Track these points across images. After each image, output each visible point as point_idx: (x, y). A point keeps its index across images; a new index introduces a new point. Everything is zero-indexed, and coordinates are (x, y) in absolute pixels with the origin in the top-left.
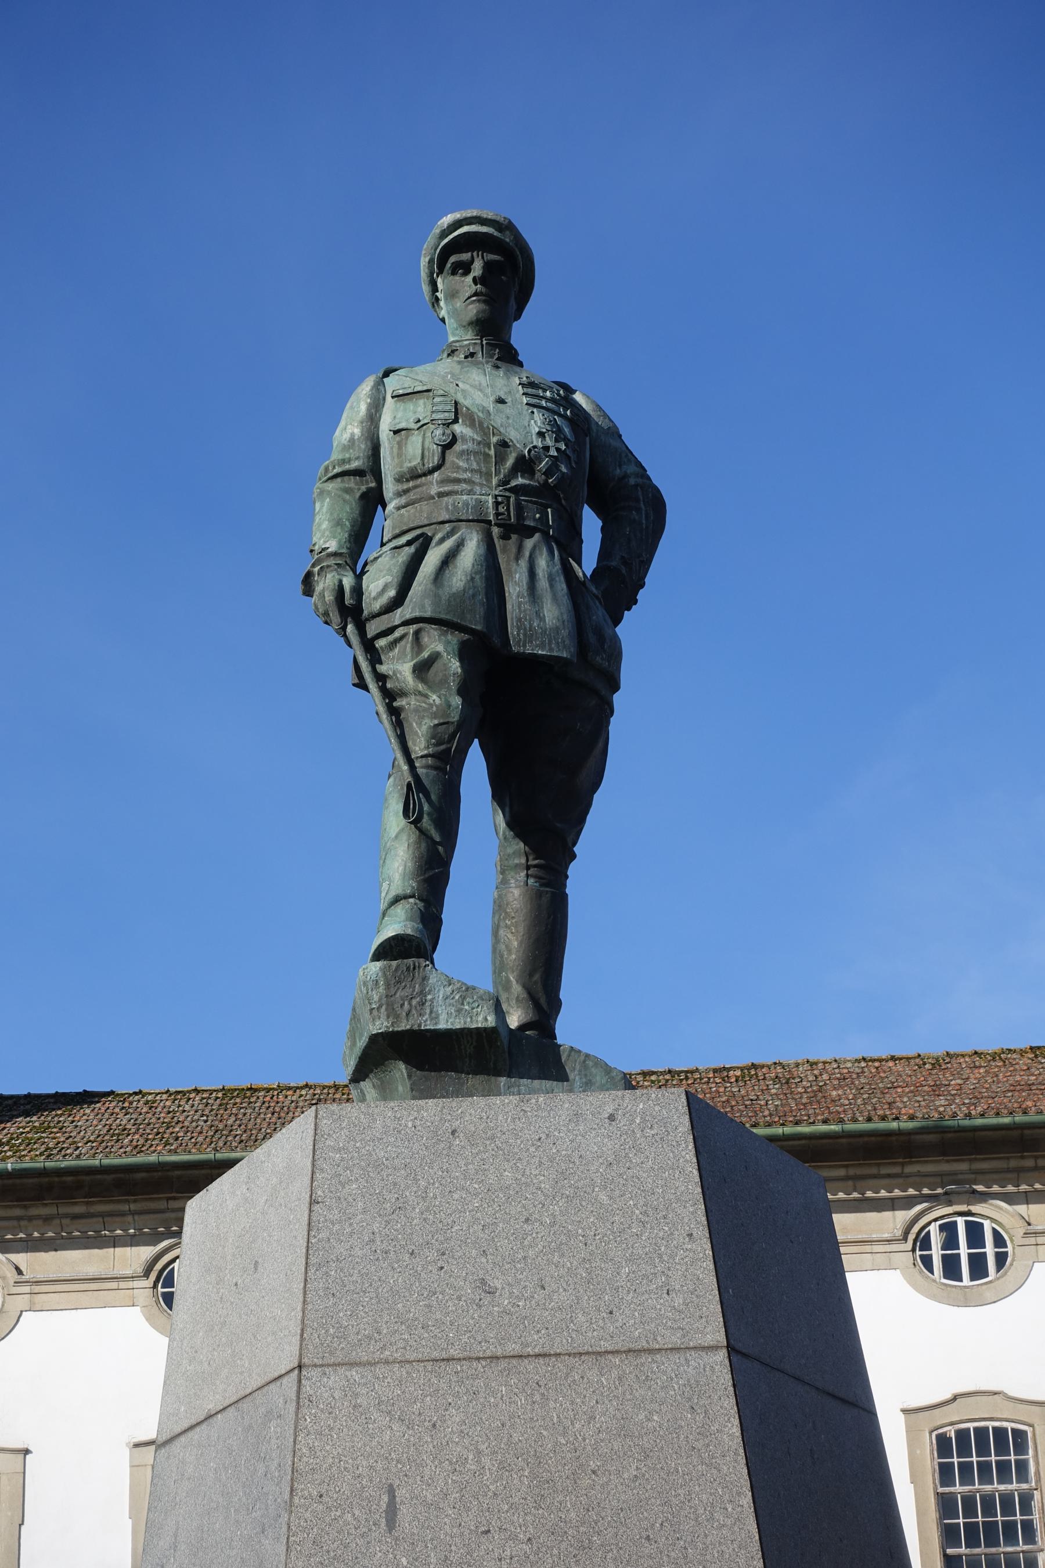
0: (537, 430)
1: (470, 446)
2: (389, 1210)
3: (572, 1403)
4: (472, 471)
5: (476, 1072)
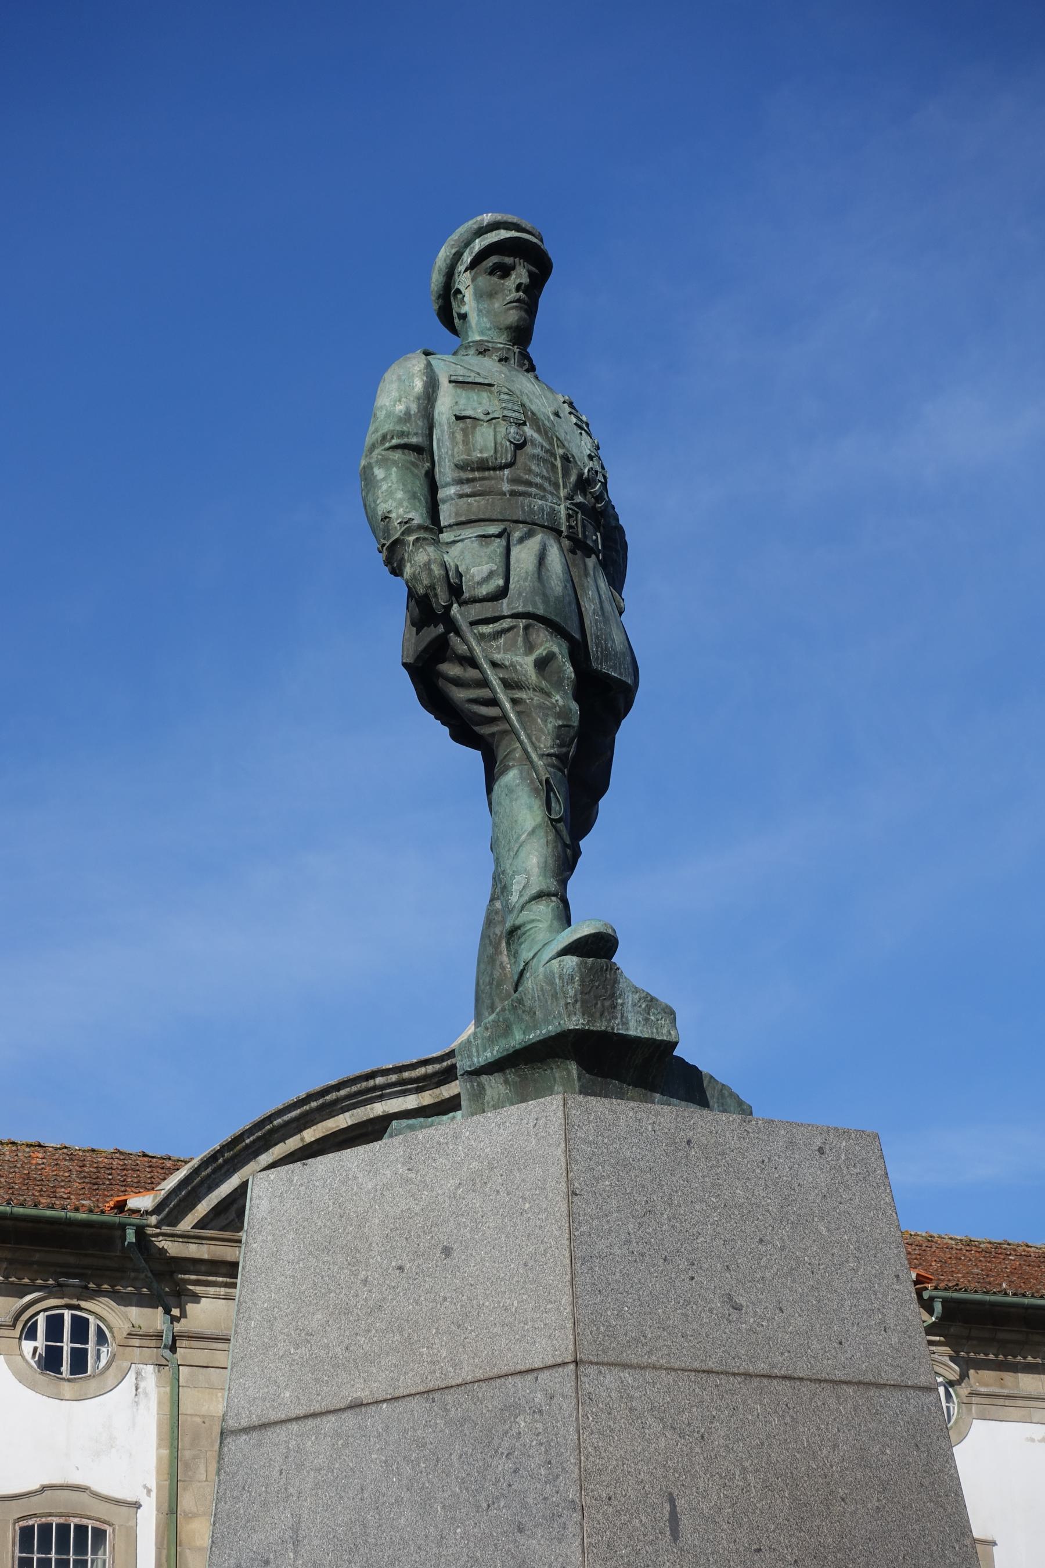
0: (589, 452)
1: (537, 451)
2: (641, 1212)
3: (818, 1428)
4: (542, 477)
5: (636, 1085)
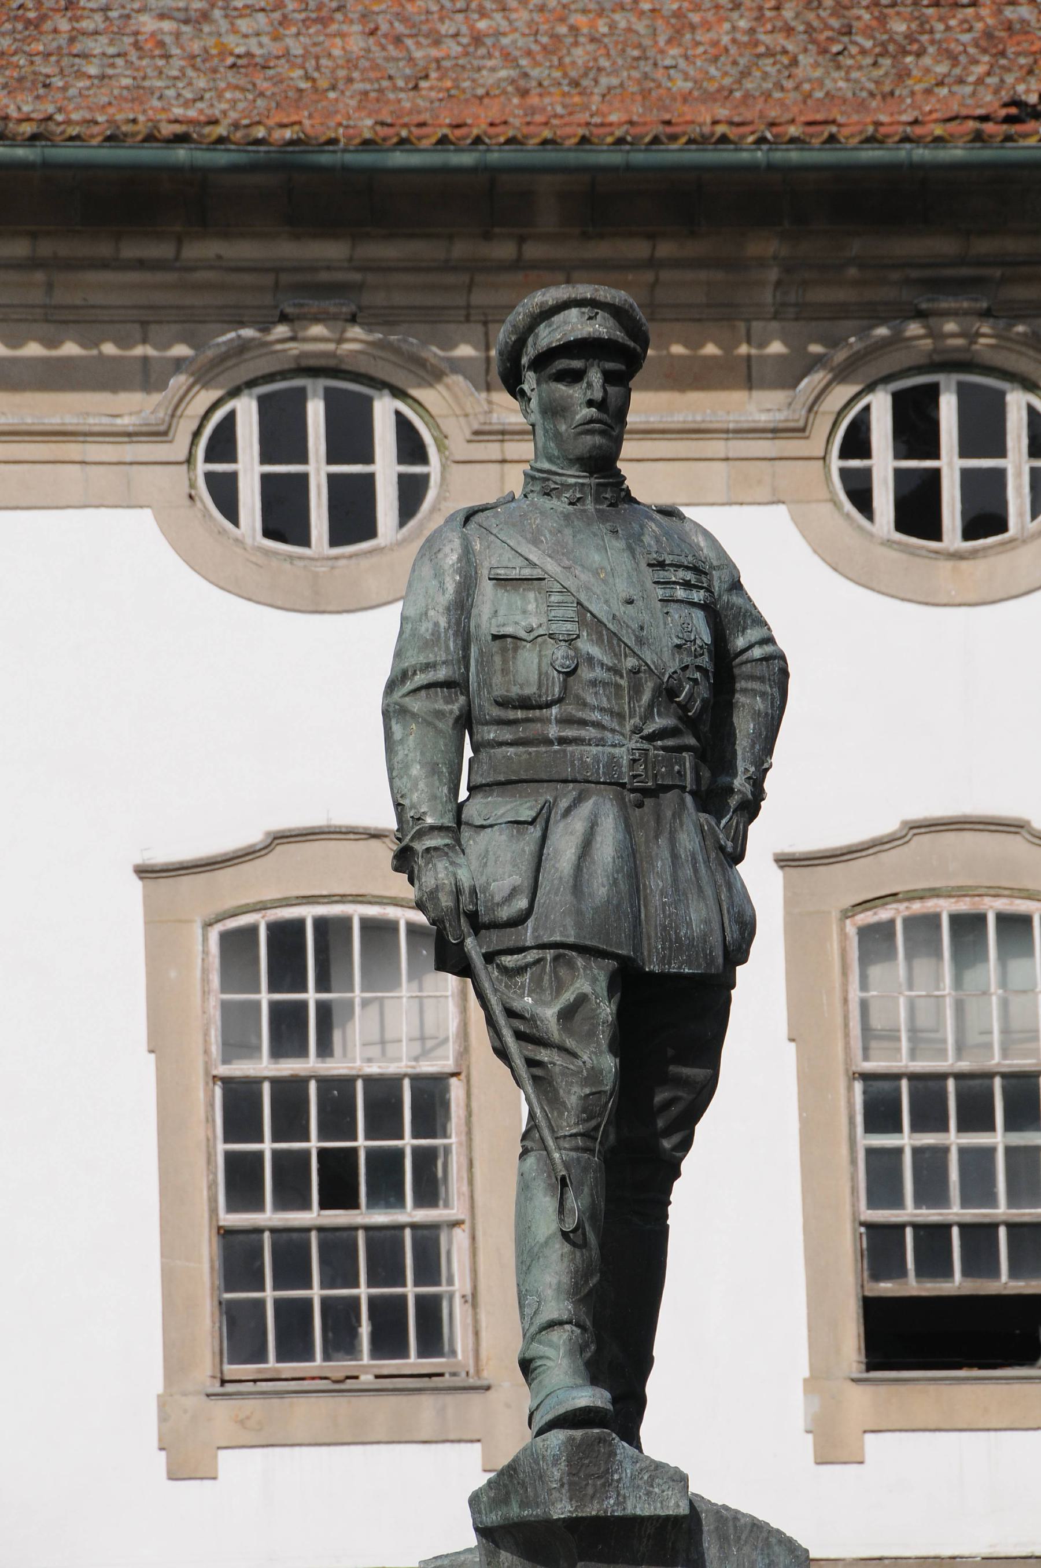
1: (599, 673)
4: (602, 710)
